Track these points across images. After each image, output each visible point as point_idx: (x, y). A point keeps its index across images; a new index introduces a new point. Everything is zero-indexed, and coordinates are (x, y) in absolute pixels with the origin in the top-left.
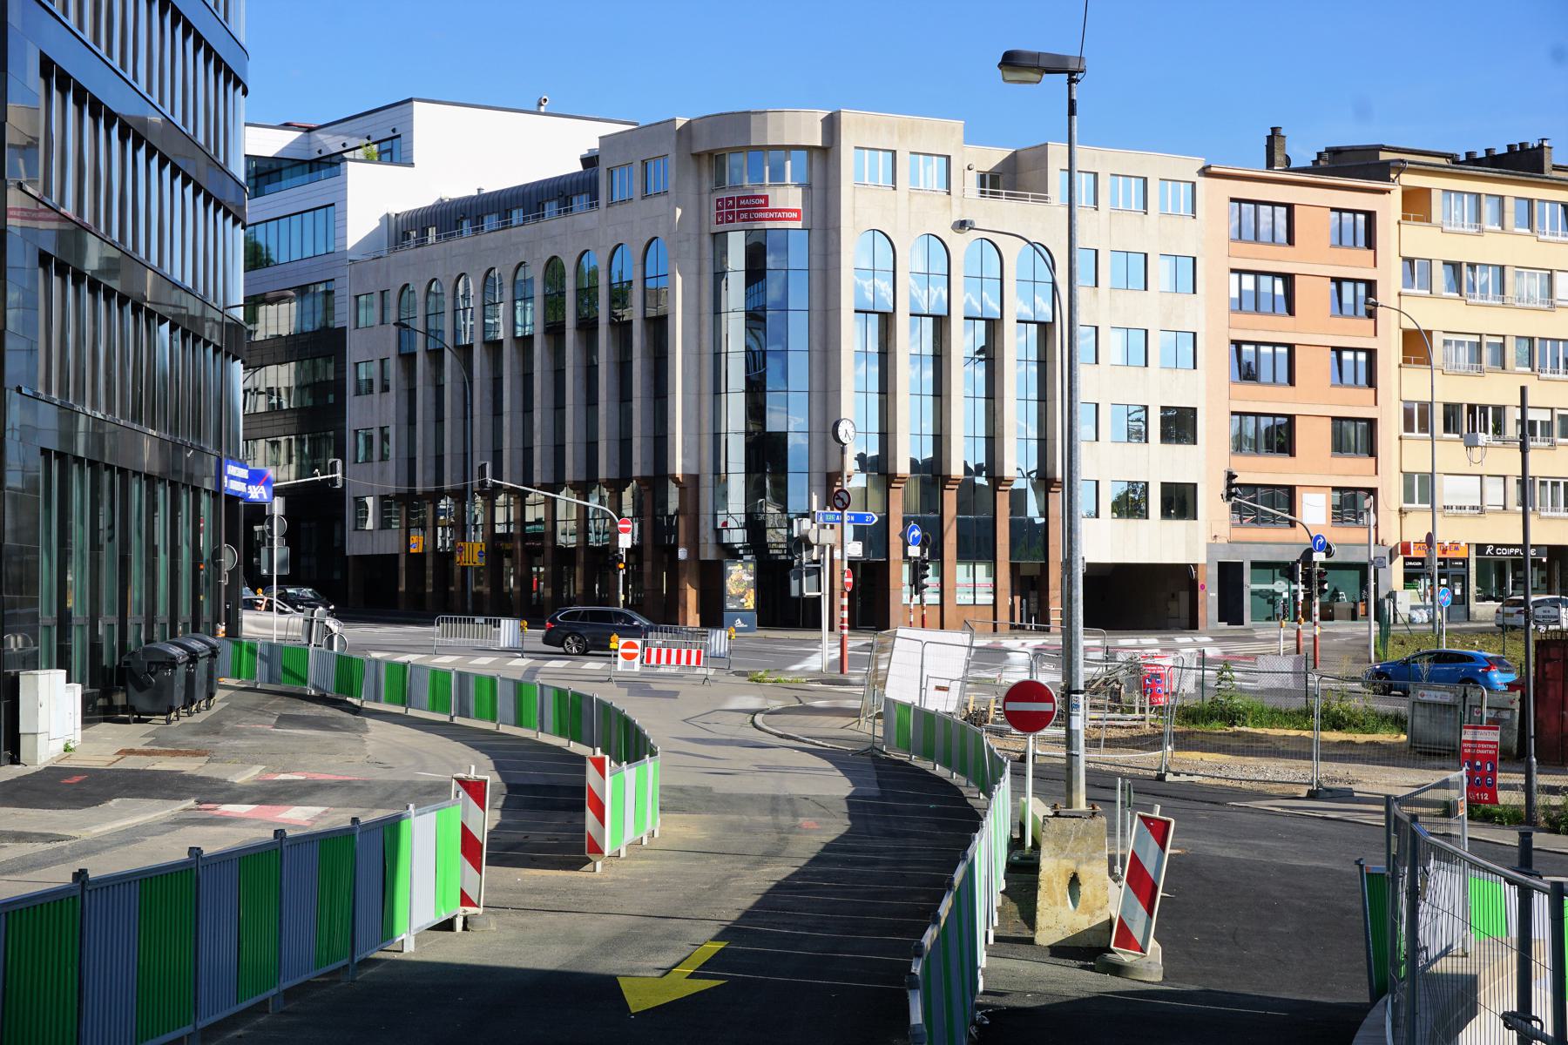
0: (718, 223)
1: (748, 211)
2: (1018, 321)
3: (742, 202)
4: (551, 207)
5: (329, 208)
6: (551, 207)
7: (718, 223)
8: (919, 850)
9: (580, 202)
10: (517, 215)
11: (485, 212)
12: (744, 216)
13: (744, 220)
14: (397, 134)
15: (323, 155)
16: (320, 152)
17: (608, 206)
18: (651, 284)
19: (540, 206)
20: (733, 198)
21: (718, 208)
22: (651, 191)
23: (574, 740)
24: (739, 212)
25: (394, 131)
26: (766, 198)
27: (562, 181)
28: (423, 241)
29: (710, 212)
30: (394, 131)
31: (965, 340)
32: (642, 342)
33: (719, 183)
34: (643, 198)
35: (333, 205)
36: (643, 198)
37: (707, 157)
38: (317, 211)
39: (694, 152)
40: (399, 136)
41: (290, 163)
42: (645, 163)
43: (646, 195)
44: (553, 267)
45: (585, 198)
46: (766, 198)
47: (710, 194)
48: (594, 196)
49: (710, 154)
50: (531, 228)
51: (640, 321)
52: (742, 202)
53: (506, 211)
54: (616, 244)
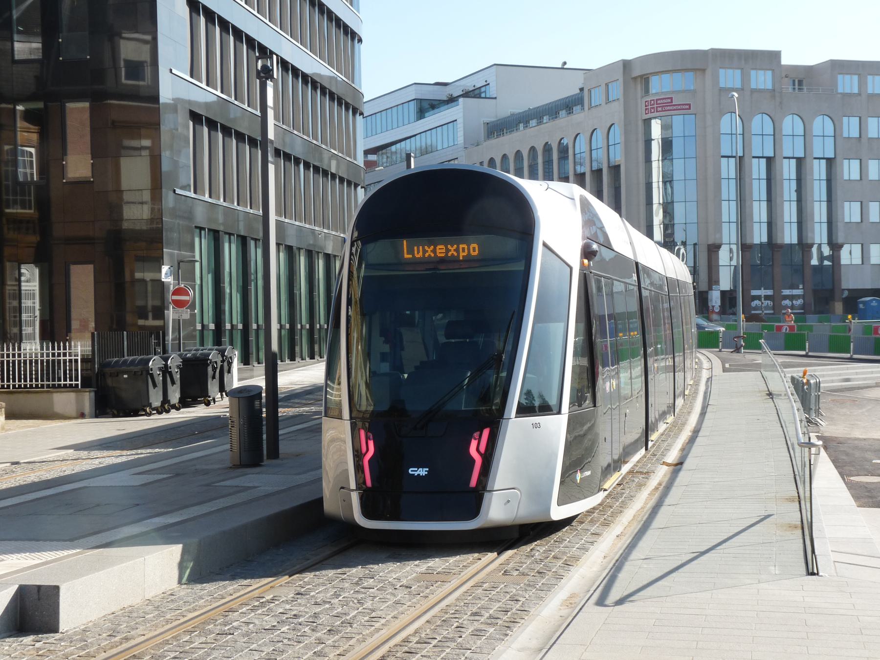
0: (646, 114)
1: (662, 107)
2: (495, 98)
3: (658, 102)
4: (563, 113)
5: (455, 122)
6: (563, 113)
7: (646, 114)
8: (791, 490)
9: (577, 109)
10: (545, 119)
11: (530, 118)
12: (660, 109)
13: (660, 111)
14: (487, 83)
15: (476, 88)
16: (474, 86)
17: (589, 109)
18: (578, 156)
19: (541, 118)
20: (654, 100)
21: (646, 106)
22: (611, 99)
23: (503, 416)
24: (657, 107)
25: (486, 81)
26: (671, 98)
27: (550, 106)
28: (541, 122)
29: (641, 108)
30: (486, 81)
31: (788, 170)
32: (608, 179)
33: (647, 91)
34: (606, 104)
35: (456, 120)
36: (606, 104)
37: (639, 79)
38: (443, 126)
39: (633, 76)
40: (489, 84)
41: (438, 102)
42: (607, 85)
43: (608, 101)
44: (547, 148)
45: (579, 107)
46: (671, 98)
47: (641, 98)
48: (583, 105)
49: (641, 76)
50: (552, 124)
51: (572, 176)
52: (658, 102)
53: (527, 121)
54: (593, 129)
